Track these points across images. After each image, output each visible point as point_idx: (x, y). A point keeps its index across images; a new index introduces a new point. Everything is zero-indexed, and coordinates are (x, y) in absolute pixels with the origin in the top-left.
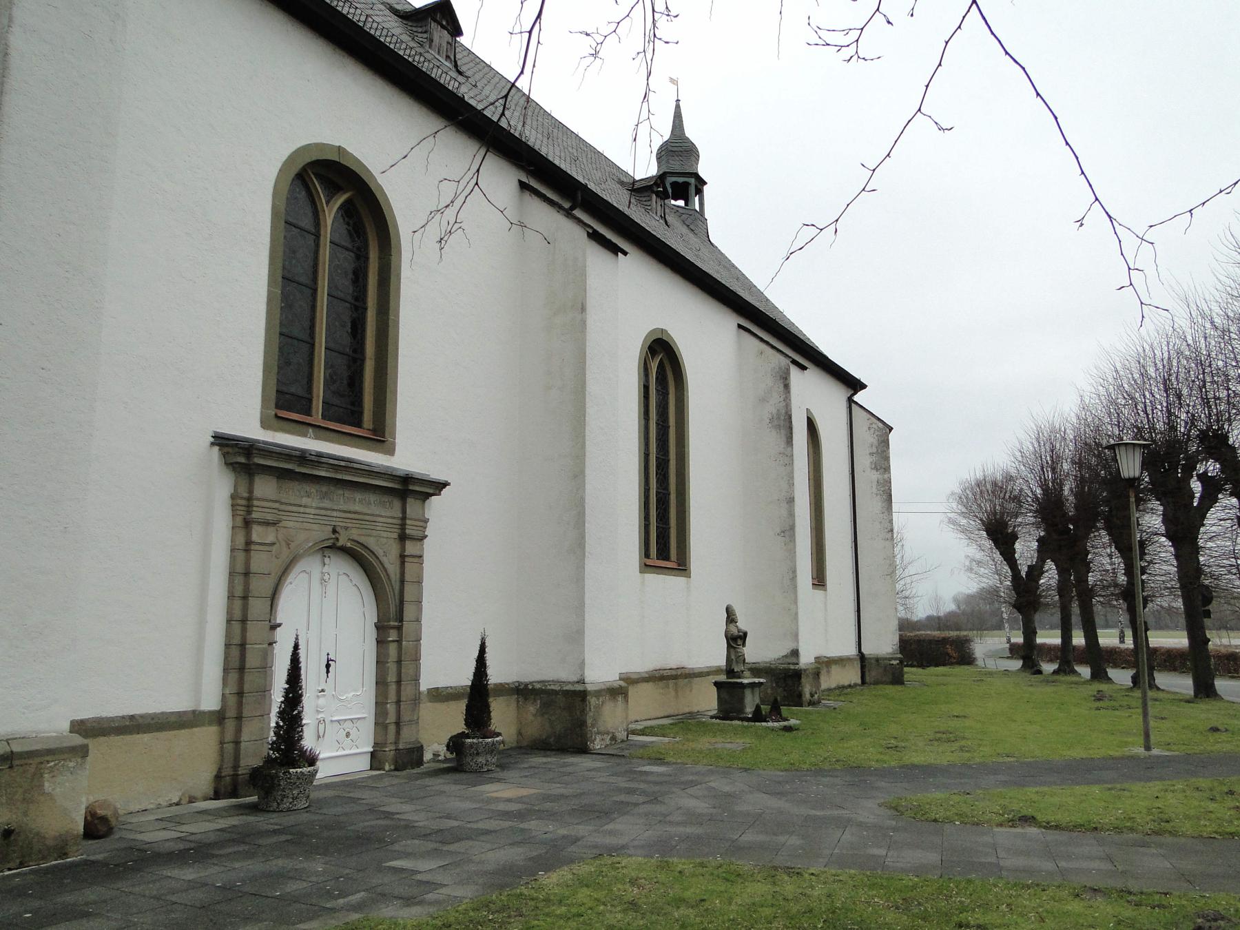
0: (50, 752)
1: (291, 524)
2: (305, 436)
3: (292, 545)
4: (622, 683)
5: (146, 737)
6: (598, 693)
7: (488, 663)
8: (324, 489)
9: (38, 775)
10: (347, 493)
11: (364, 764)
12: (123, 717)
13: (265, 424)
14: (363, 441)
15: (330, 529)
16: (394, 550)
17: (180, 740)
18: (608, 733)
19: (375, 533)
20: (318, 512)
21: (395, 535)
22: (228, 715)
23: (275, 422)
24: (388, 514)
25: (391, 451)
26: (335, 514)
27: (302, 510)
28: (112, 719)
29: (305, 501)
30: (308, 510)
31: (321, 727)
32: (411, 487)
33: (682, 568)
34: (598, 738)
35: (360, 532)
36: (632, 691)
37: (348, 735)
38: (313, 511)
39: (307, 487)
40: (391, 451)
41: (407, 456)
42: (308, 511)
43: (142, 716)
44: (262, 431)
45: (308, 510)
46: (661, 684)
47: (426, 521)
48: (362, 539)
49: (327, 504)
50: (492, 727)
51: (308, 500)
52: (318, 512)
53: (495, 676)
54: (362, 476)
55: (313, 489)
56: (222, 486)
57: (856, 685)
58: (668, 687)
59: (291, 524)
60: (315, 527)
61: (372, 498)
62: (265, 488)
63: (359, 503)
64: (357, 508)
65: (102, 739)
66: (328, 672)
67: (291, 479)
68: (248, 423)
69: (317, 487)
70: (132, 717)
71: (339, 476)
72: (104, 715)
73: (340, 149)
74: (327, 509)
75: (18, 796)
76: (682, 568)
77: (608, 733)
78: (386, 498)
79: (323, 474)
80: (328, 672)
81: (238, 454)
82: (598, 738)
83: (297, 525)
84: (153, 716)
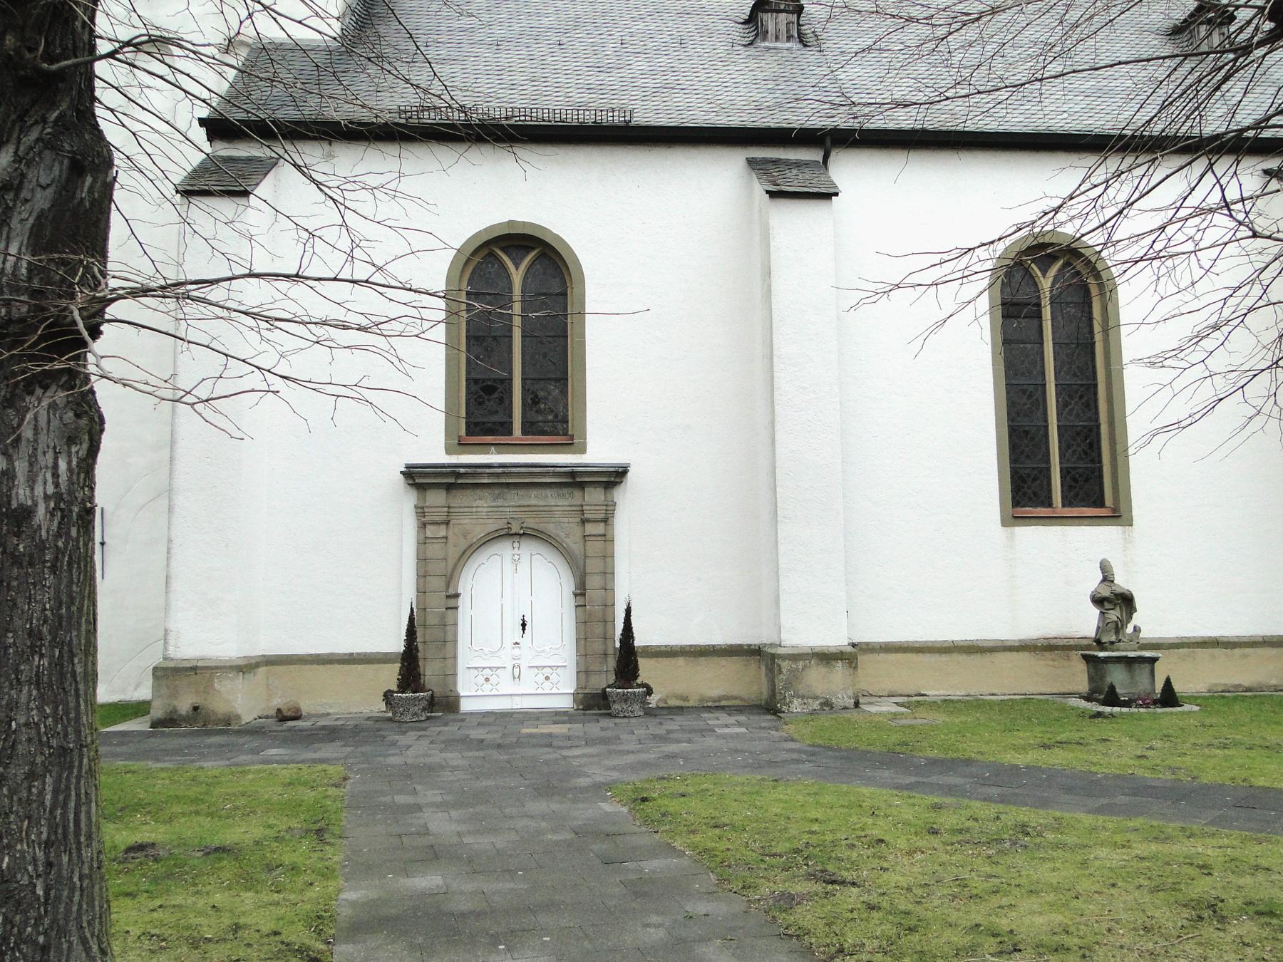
0: (217, 668)
2: (488, 453)
4: (850, 649)
5: (360, 667)
6: (795, 657)
8: (497, 492)
9: (211, 679)
10: (521, 492)
14: (551, 448)
16: (577, 531)
18: (816, 698)
28: (338, 654)
29: (479, 503)
31: (517, 670)
33: (1118, 515)
34: (796, 702)
36: (862, 658)
37: (487, 680)
39: (479, 492)
40: (582, 450)
41: (598, 450)
42: (480, 511)
46: (1047, 654)
55: (486, 493)
56: (408, 500)
57: (166, 649)
58: (1068, 658)
61: (549, 492)
62: (437, 498)
63: (533, 498)
64: (533, 502)
66: (524, 629)
68: (432, 449)
73: (511, 223)
75: (201, 689)
76: (1118, 515)
77: (816, 698)
78: (565, 491)
80: (524, 629)
81: (416, 477)
82: (796, 702)
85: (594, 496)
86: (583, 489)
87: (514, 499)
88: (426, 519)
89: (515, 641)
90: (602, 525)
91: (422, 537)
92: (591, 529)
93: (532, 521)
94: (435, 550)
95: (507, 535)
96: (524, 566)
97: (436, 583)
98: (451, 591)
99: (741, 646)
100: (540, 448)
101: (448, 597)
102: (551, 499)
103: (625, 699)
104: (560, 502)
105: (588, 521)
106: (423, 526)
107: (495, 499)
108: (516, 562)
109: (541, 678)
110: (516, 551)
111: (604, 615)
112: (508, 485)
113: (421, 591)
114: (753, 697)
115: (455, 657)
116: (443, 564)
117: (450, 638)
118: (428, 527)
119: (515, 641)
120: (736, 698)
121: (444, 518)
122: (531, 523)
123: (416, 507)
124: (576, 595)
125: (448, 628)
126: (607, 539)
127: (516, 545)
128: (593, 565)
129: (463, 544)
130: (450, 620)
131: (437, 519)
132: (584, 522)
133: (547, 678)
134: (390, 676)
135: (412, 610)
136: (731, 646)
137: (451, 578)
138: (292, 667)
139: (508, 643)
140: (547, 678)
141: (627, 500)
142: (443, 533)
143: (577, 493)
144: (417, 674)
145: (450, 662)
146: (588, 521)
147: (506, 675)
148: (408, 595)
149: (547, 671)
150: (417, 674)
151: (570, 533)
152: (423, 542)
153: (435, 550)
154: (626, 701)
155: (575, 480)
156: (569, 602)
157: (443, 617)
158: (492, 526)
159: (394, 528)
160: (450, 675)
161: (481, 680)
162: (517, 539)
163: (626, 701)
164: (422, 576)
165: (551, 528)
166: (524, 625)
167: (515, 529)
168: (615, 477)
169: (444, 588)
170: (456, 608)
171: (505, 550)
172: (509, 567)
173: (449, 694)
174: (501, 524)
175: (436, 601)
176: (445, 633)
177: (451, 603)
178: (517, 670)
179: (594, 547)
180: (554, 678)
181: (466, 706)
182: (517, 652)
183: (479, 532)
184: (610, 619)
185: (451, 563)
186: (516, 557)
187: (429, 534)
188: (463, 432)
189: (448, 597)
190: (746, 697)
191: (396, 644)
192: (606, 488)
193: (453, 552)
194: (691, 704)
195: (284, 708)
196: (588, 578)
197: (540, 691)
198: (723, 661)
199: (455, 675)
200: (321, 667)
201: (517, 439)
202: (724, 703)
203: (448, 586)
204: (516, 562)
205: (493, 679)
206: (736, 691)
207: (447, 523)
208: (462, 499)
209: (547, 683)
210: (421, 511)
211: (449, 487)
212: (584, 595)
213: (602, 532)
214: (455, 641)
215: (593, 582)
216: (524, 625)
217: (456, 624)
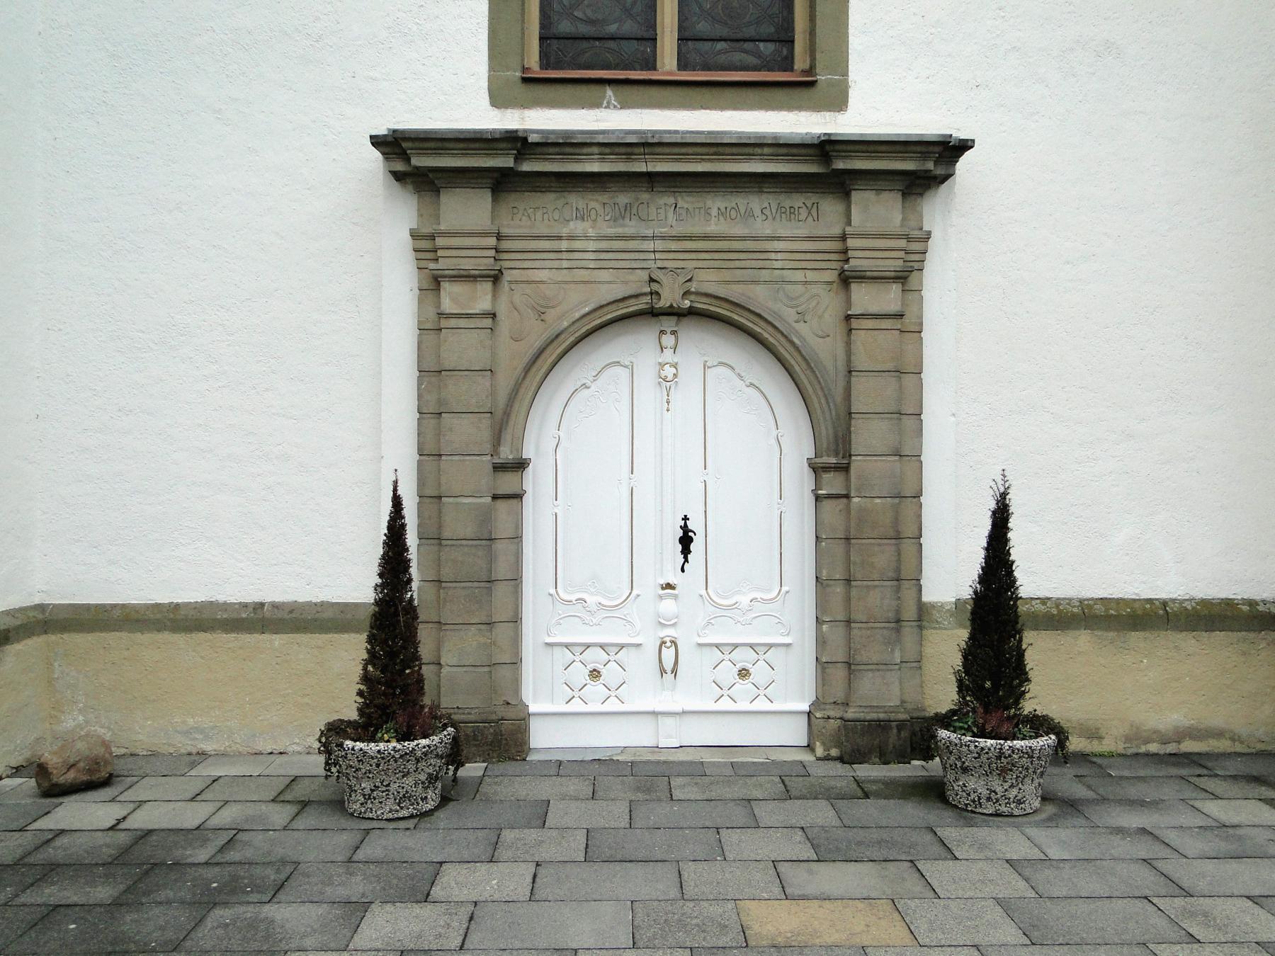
1: (542, 275)
2: (596, 105)
3: (551, 315)
5: (278, 640)
7: (1015, 555)
8: (623, 199)
11: (795, 733)
12: (1150, 601)
13: (499, 99)
15: (644, 275)
16: (828, 304)
17: (303, 647)
19: (765, 275)
20: (604, 245)
21: (832, 276)
22: (905, 616)
23: (522, 89)
24: (802, 231)
25: (838, 101)
26: (649, 245)
27: (564, 245)
28: (225, 606)
29: (577, 227)
30: (578, 245)
31: (668, 654)
32: (840, 165)
35: (727, 275)
37: (595, 674)
38: (592, 245)
39: (576, 200)
40: (838, 101)
41: (879, 100)
42: (579, 248)
43: (275, 606)
44: (495, 113)
45: (578, 245)
47: (928, 236)
48: (721, 291)
49: (631, 227)
50: (1028, 706)
51: (583, 223)
52: (604, 245)
53: (1034, 579)
54: (749, 157)
55: (593, 202)
56: (396, 218)
59: (542, 275)
60: (604, 275)
61: (755, 202)
62: (468, 211)
63: (715, 215)
64: (713, 228)
65: (202, 635)
66: (686, 551)
67: (535, 190)
68: (460, 98)
69: (605, 197)
70: (41, 607)
71: (640, 167)
72: (221, 598)
74: (632, 238)
79: (595, 167)
80: (686, 551)
81: (414, 160)
83: (564, 276)
84: (293, 607)
85: (875, 211)
86: (846, 195)
87: (669, 216)
88: (442, 264)
89: (666, 577)
90: (895, 288)
91: (431, 312)
92: (865, 298)
93: (712, 276)
94: (464, 347)
95: (650, 313)
96: (687, 395)
97: (466, 432)
98: (506, 454)
99: (1228, 603)
100: (729, 93)
101: (499, 468)
102: (759, 217)
103: (1004, 766)
104: (783, 229)
105: (862, 277)
106: (433, 283)
107: (618, 218)
108: (666, 383)
109: (728, 673)
110: (668, 355)
111: (896, 521)
112: (652, 180)
113: (430, 454)
114: (1260, 733)
115: (516, 620)
116: (484, 382)
117: (502, 570)
118: (445, 285)
119: (666, 577)
120: (1219, 734)
121: (484, 263)
122: (709, 281)
123: (415, 235)
124: (817, 469)
125: (499, 546)
126: (906, 324)
127: (668, 340)
128: (867, 394)
129: (536, 335)
130: (502, 527)
131: (467, 265)
132: (845, 280)
133: (744, 673)
134: (350, 654)
135: (397, 502)
136: (1205, 603)
137: (505, 419)
138: (112, 638)
139: (648, 583)
140: (744, 673)
141: (964, 235)
142: (484, 304)
143: (830, 208)
144: (415, 679)
145: (502, 632)
146: (862, 277)
147: (642, 664)
148: (398, 459)
149: (744, 657)
150: (415, 679)
151: (808, 309)
152: (433, 327)
153: (464, 347)
154: (1003, 772)
155: (831, 170)
156: (799, 483)
157: (486, 518)
158: (612, 286)
159: (359, 283)
160: (504, 665)
161: (579, 674)
162: (668, 323)
163: (1003, 772)
164: (432, 414)
165: (760, 296)
166: (686, 541)
167: (670, 296)
168: (928, 163)
169: (487, 448)
170: (518, 496)
171: (640, 353)
172: (648, 393)
173: (502, 712)
174: (636, 283)
175: (466, 479)
176: (491, 559)
177: (506, 483)
178: (668, 654)
179: (872, 346)
180: (760, 672)
181: (545, 738)
182: (668, 606)
183: (576, 303)
184: (909, 531)
185: (504, 382)
186: (669, 371)
187: (447, 305)
188: (533, 60)
189: (499, 468)
190: (1243, 731)
191: (358, 584)
192: (906, 194)
193: (511, 356)
194: (1107, 745)
195: (51, 758)
196: (857, 424)
197: (725, 705)
198: (1188, 642)
199: (516, 663)
200: (180, 639)
201: (670, 73)
202: (1189, 746)
203: (497, 441)
204: (666, 383)
205: (611, 673)
206: (1216, 719)
207: (496, 278)
208: (533, 216)
209: (743, 687)
210: (426, 245)
211: (501, 183)
212: (845, 469)
213: (894, 307)
214: (516, 581)
215: (869, 436)
216: (686, 541)
217: (517, 538)
